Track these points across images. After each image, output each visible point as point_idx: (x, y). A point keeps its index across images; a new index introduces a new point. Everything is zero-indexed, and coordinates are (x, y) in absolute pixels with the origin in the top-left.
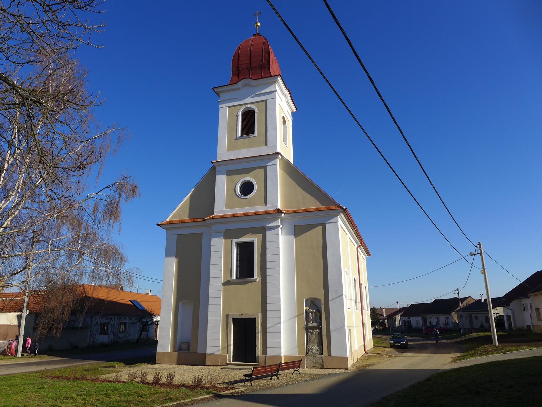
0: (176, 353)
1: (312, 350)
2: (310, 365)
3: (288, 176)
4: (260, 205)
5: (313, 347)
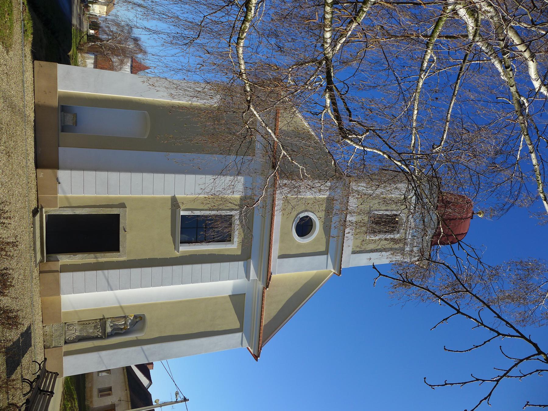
0: (55, 103)
1: (71, 330)
2: (48, 330)
3: (308, 280)
4: (280, 249)
5: (75, 331)
